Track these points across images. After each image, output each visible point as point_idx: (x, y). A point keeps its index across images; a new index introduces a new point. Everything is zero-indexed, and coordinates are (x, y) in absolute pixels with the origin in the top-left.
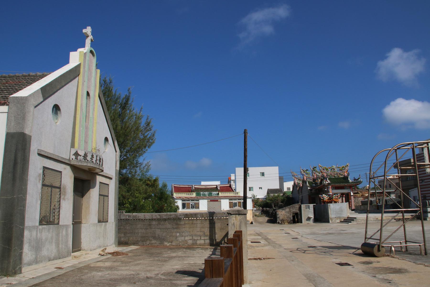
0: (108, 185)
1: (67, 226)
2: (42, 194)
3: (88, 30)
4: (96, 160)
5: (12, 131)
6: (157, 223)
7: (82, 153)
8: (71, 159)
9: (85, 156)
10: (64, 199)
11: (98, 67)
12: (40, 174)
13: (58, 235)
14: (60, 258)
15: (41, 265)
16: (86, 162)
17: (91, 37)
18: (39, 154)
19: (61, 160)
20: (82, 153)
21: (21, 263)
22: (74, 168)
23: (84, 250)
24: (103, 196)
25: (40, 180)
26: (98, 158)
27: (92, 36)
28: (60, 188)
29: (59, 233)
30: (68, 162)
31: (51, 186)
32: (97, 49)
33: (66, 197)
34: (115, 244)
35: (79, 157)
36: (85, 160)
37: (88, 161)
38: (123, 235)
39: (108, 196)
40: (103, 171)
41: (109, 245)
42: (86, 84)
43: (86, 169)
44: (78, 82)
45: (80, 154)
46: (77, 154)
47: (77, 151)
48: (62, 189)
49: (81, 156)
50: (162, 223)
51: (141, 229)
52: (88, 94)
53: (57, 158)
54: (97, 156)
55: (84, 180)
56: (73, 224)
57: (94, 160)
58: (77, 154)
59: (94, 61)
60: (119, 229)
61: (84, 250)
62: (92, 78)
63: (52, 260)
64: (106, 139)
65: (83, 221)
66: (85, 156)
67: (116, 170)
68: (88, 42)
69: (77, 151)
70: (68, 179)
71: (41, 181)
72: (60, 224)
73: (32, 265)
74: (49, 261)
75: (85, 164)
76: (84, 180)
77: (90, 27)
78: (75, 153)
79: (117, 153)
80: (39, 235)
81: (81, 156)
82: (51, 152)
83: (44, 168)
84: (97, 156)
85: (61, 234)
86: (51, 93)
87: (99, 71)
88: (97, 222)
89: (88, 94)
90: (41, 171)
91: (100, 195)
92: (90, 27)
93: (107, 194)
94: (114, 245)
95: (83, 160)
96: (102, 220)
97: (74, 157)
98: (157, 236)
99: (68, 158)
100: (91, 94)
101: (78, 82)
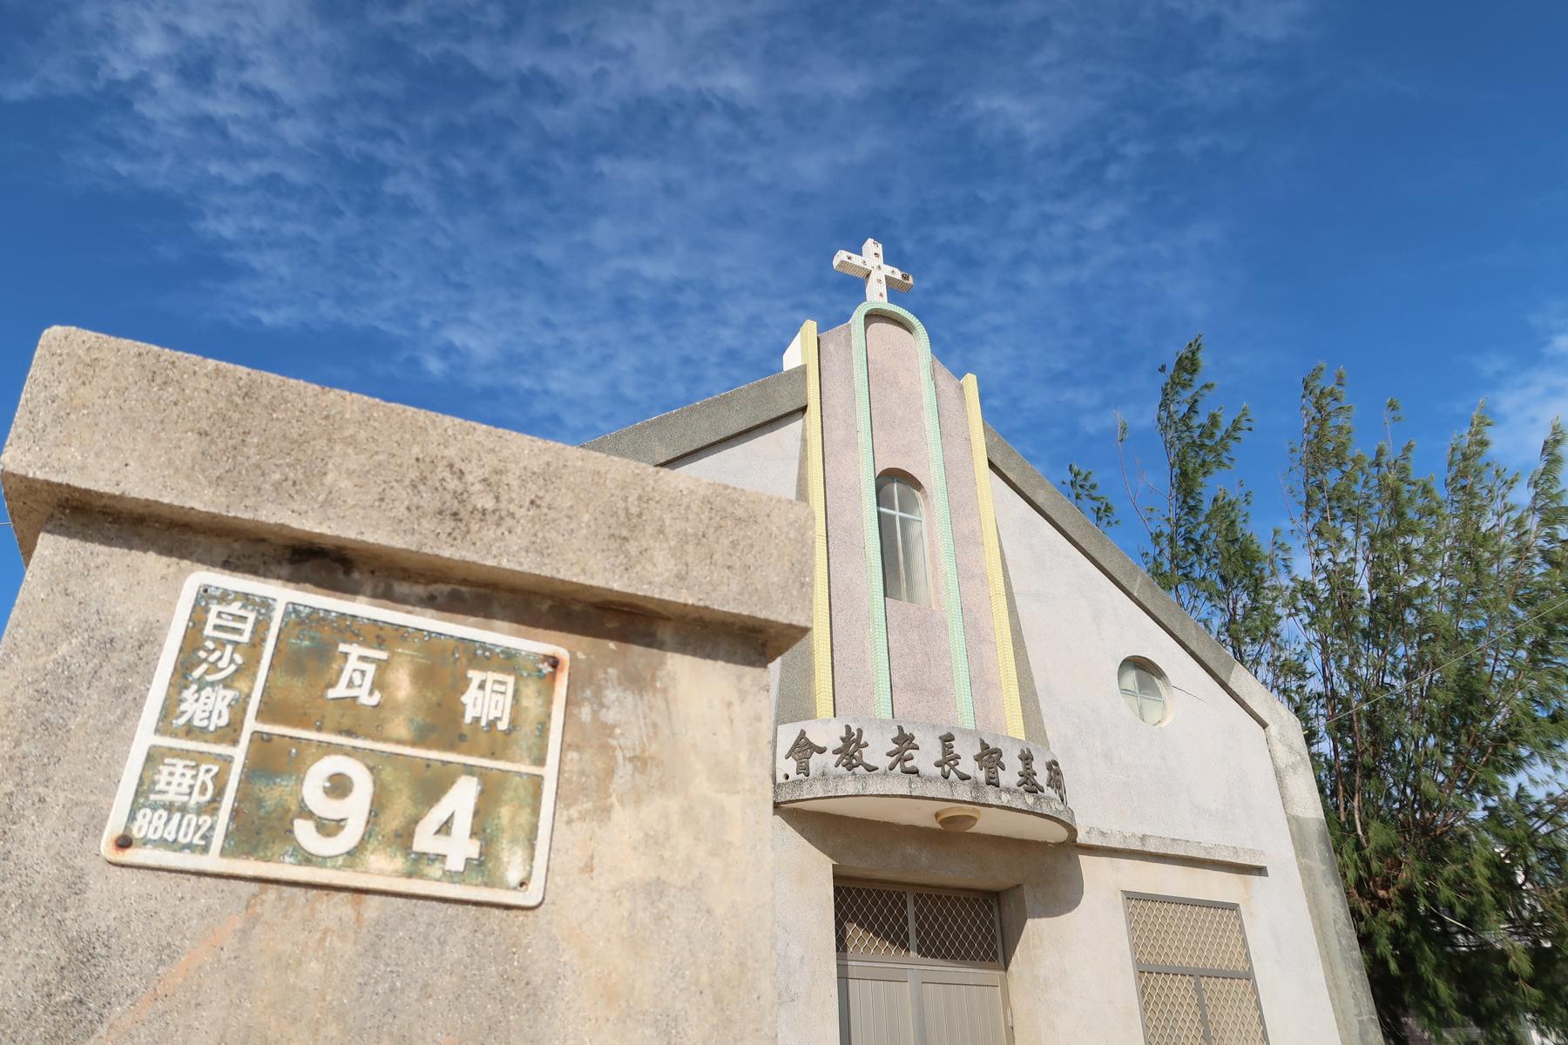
0: (1233, 907)
4: (949, 758)
20: (827, 734)
26: (967, 752)
35: (816, 761)
36: (850, 767)
37: (871, 769)
39: (1248, 976)
43: (922, 816)
47: (803, 733)
49: (822, 751)
54: (947, 739)
57: (926, 757)
58: (803, 748)
59: (920, 342)
69: (803, 733)
75: (850, 787)
77: (870, 241)
78: (796, 744)
81: (822, 751)
84: (947, 739)
93: (1240, 966)
95: (842, 770)
100: (931, 474)
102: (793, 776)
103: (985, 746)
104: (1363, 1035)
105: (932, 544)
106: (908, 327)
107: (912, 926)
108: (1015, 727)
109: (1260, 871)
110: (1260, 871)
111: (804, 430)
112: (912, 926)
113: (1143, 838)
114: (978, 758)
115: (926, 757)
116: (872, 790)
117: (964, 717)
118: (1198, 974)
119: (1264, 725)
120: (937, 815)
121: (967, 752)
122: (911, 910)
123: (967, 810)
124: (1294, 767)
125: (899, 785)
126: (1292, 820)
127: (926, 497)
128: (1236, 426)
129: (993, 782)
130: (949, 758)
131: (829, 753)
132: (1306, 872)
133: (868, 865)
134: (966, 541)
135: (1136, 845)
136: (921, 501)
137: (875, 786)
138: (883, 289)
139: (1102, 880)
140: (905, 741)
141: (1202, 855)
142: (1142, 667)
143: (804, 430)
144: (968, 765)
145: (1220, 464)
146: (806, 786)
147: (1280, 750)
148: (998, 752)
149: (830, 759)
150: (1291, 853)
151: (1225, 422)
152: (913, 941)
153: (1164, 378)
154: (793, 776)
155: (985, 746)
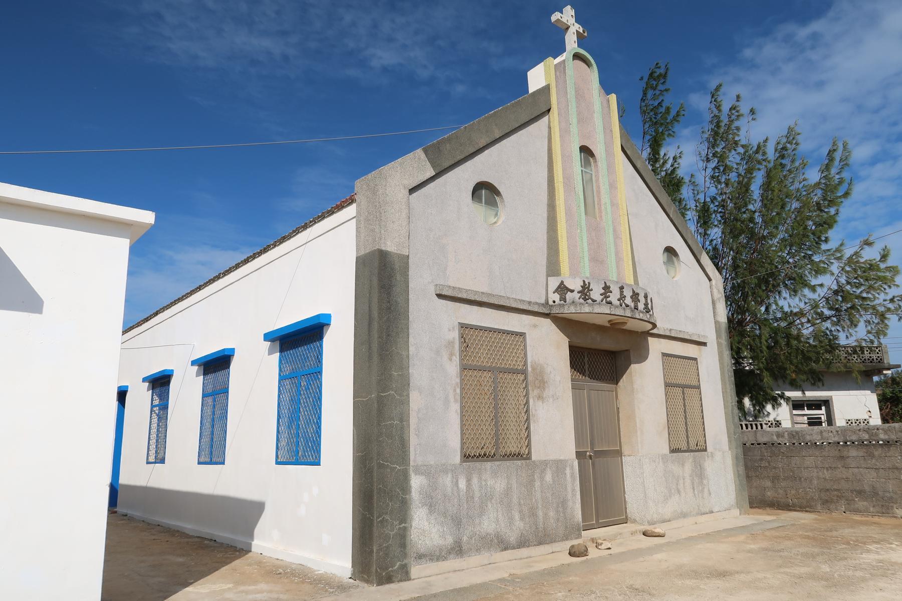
0: (695, 359)
1: (559, 466)
2: (462, 389)
3: (567, 16)
4: (622, 298)
5: (362, 253)
6: (861, 454)
7: (575, 284)
8: (551, 303)
9: (585, 291)
10: (540, 397)
11: (607, 86)
12: (451, 343)
13: (531, 482)
14: (540, 543)
15: (473, 560)
16: (590, 305)
17: (575, 28)
18: (440, 296)
19: (514, 306)
20: (575, 284)
21: (405, 555)
22: (565, 324)
23: (634, 521)
24: (681, 388)
25: (452, 354)
26: (628, 293)
27: (577, 26)
28: (524, 372)
29: (533, 480)
30: (546, 311)
31: (491, 369)
32: (595, 48)
33: (548, 393)
34: (739, 505)
35: (569, 296)
36: (585, 299)
37: (594, 301)
38: (768, 484)
39: (698, 387)
40: (654, 326)
41: (715, 510)
42: (574, 129)
43: (603, 321)
44: (550, 128)
45: (571, 288)
46: (562, 289)
47: (562, 282)
48: (530, 378)
49: (572, 291)
50: (878, 452)
51: (816, 467)
52: (586, 151)
53: (501, 303)
54: (622, 288)
55: (603, 353)
56: (580, 455)
57: (614, 297)
58: (562, 289)
59: (593, 75)
60: (747, 467)
61: (634, 521)
62: (595, 115)
63: (514, 548)
64: (670, 251)
65: (626, 450)
66: (585, 291)
67: (717, 323)
68: (571, 42)
69: (562, 282)
70: (548, 349)
71: (456, 359)
72: (534, 458)
73: (445, 559)
74: (506, 549)
75: (587, 309)
76: (603, 353)
77: (569, 7)
78: (559, 287)
79: (714, 282)
80: (462, 484)
81: (572, 291)
82: (485, 289)
83: (463, 326)
84: (622, 288)
85: (537, 484)
86: (459, 158)
87: (613, 97)
88: (666, 450)
89: (586, 151)
90: (455, 335)
91: (667, 385)
92: (569, 7)
93: (695, 383)
94: (736, 512)
95: (582, 301)
96: (687, 442)
97: (556, 297)
98: (867, 488)
99: (543, 301)
100: (599, 150)
101: (550, 128)
102: (557, 301)
103: (634, 291)
104: (732, 410)
105: (598, 187)
106: (588, 64)
107: (587, 366)
108: (630, 280)
109: (704, 344)
110: (704, 344)
111: (549, 122)
112: (587, 366)
113: (671, 330)
114: (631, 297)
115: (614, 297)
116: (596, 311)
117: (612, 276)
118: (684, 387)
119: (710, 280)
120: (609, 321)
121: (628, 293)
122: (586, 359)
123: (622, 320)
124: (719, 299)
125: (606, 309)
126: (716, 322)
127: (596, 161)
128: (678, 114)
129: (636, 308)
130: (622, 298)
131: (576, 292)
132: (719, 344)
133: (581, 342)
134: (613, 186)
135: (668, 334)
136: (592, 163)
137: (597, 309)
138: (575, 38)
139: (656, 346)
140: (607, 288)
141: (688, 338)
142: (670, 251)
143: (549, 122)
144: (628, 301)
145: (669, 135)
146: (566, 307)
147: (715, 291)
148: (638, 294)
149: (576, 296)
150: (715, 337)
151: (673, 113)
152: (587, 372)
153: (643, 84)
154: (557, 301)
155: (634, 291)
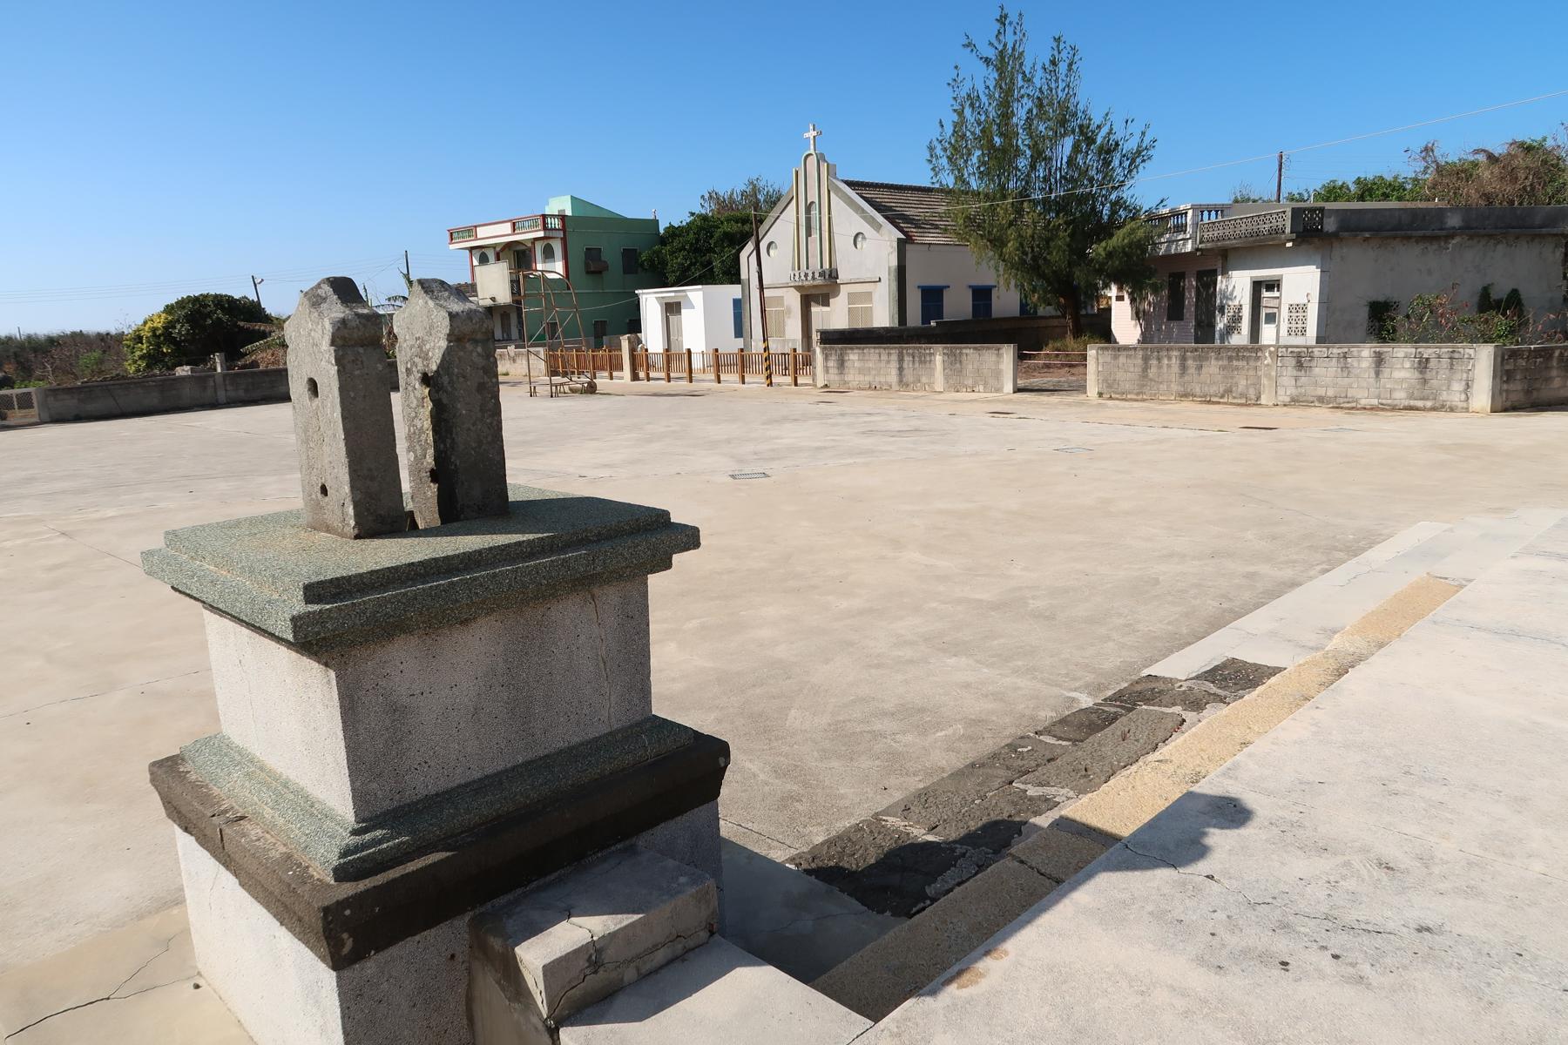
22: (797, 288)
